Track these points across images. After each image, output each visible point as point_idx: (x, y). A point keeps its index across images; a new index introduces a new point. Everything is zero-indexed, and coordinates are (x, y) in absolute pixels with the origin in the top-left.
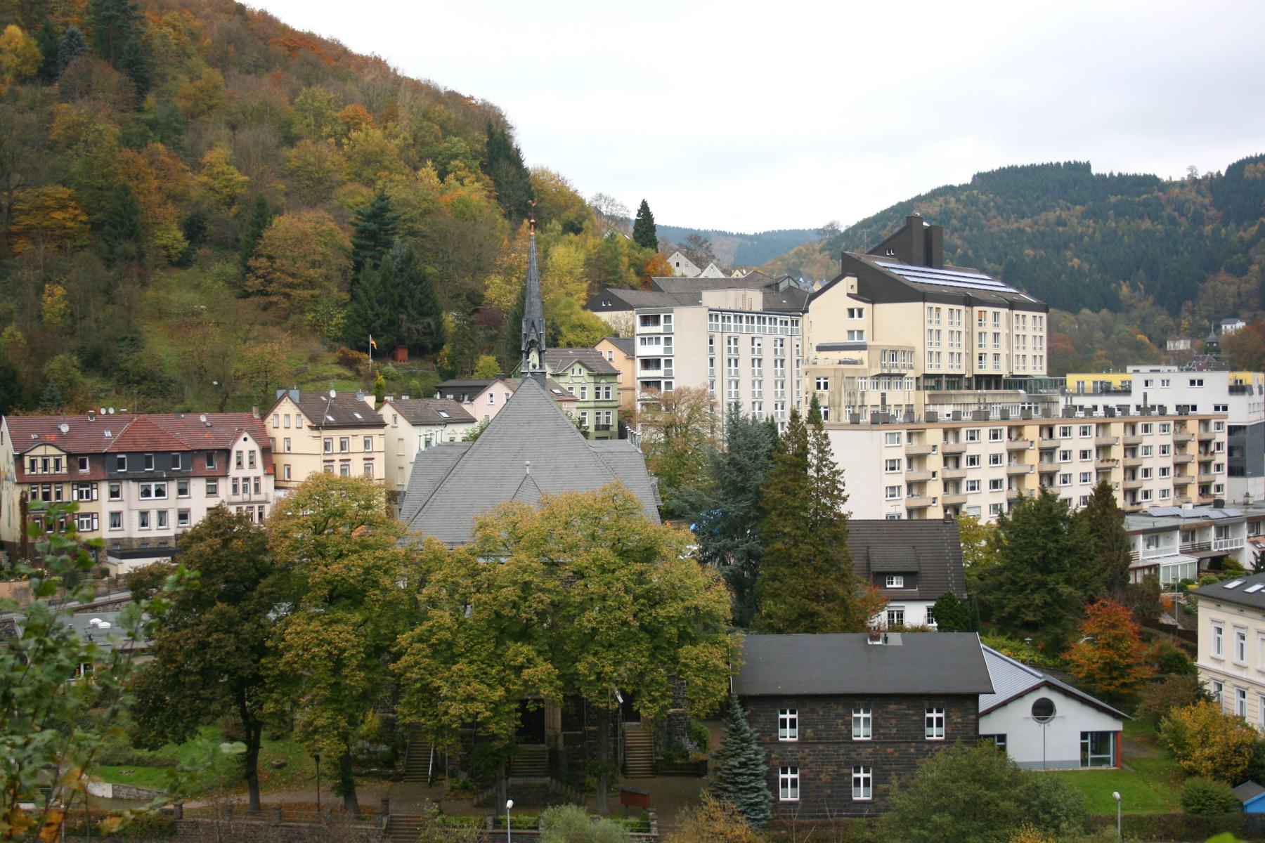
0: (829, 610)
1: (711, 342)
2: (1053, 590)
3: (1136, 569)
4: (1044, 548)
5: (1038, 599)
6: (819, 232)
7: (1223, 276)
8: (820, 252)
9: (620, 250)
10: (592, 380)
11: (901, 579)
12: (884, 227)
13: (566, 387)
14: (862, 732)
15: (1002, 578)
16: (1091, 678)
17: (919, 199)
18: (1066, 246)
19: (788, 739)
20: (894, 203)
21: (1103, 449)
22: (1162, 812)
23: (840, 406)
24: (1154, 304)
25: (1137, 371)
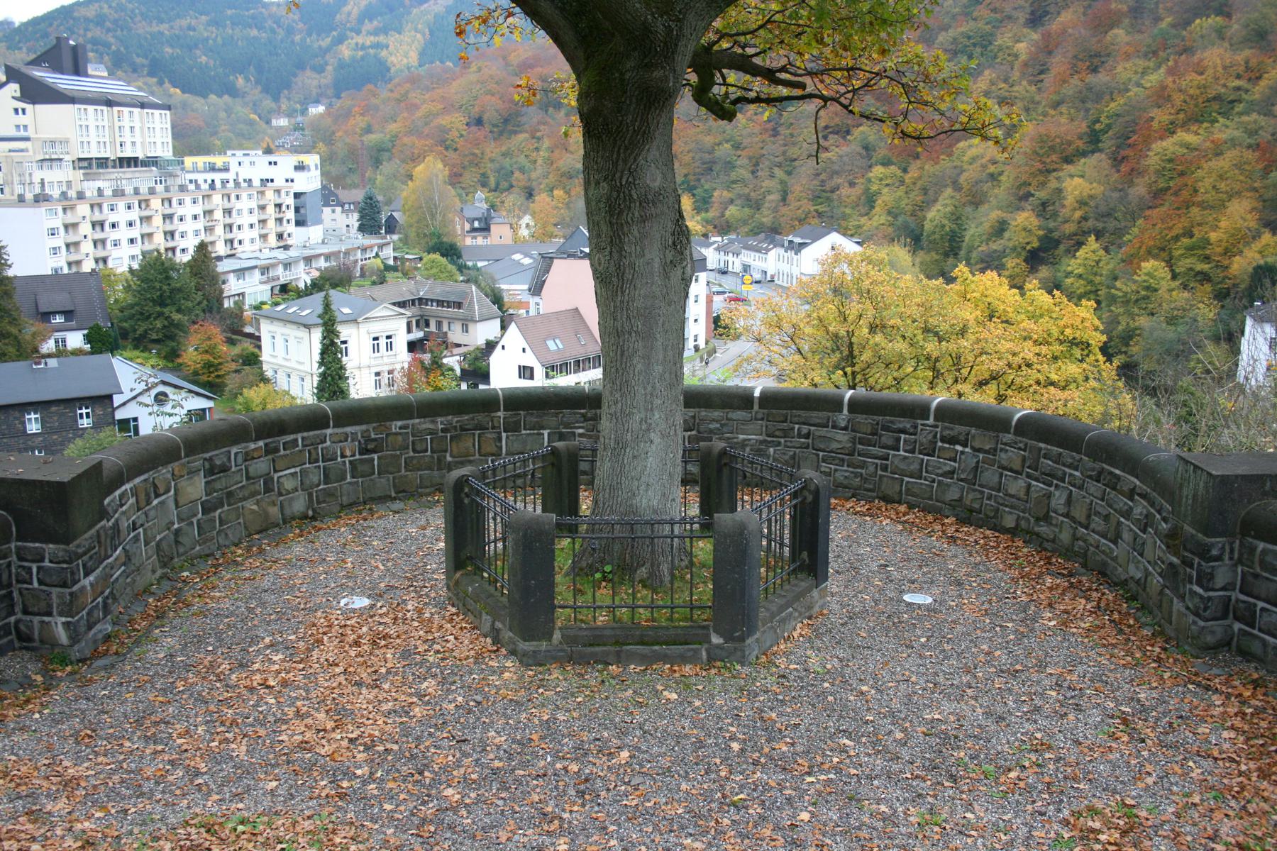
2: (169, 317)
3: (229, 297)
4: (161, 289)
5: (159, 324)
7: (308, 73)
12: (51, 25)
15: (133, 311)
16: (196, 373)
18: (196, 46)
20: (58, 6)
23: (12, 183)
24: (261, 92)
25: (234, 155)
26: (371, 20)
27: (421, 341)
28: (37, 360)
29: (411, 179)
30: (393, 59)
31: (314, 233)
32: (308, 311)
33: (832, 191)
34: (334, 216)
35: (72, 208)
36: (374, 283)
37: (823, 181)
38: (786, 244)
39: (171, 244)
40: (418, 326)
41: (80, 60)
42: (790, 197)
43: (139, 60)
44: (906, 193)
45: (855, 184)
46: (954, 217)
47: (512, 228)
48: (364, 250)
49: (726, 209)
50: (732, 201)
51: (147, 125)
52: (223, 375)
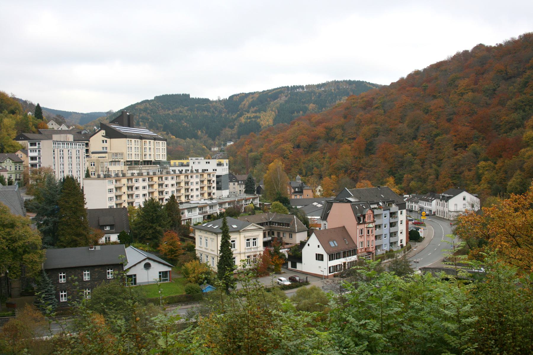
0: (81, 239)
1: (54, 151)
2: (155, 228)
3: (184, 220)
5: (150, 232)
6: (108, 113)
7: (227, 129)
8: (106, 120)
9: (29, 120)
10: (13, 164)
11: (109, 227)
13: (4, 167)
14: (86, 278)
15: (139, 226)
16: (165, 254)
17: (138, 104)
18: (182, 119)
19: (63, 282)
20: (130, 105)
21: (178, 183)
22: (181, 294)
23: (99, 171)
26: (253, 107)
27: (270, 241)
28: (91, 246)
29: (268, 170)
30: (262, 122)
31: (225, 193)
32: (217, 226)
33: (460, 173)
34: (234, 186)
35: (120, 180)
36: (250, 215)
37: (455, 169)
38: (441, 197)
39: (161, 197)
40: (269, 234)
41: (131, 121)
42: (440, 177)
43: (159, 125)
44: (497, 173)
45: (471, 170)
46: (522, 184)
47: (313, 192)
48: (246, 200)
49: (410, 183)
50: (412, 179)
51: (156, 147)
52: (178, 255)
